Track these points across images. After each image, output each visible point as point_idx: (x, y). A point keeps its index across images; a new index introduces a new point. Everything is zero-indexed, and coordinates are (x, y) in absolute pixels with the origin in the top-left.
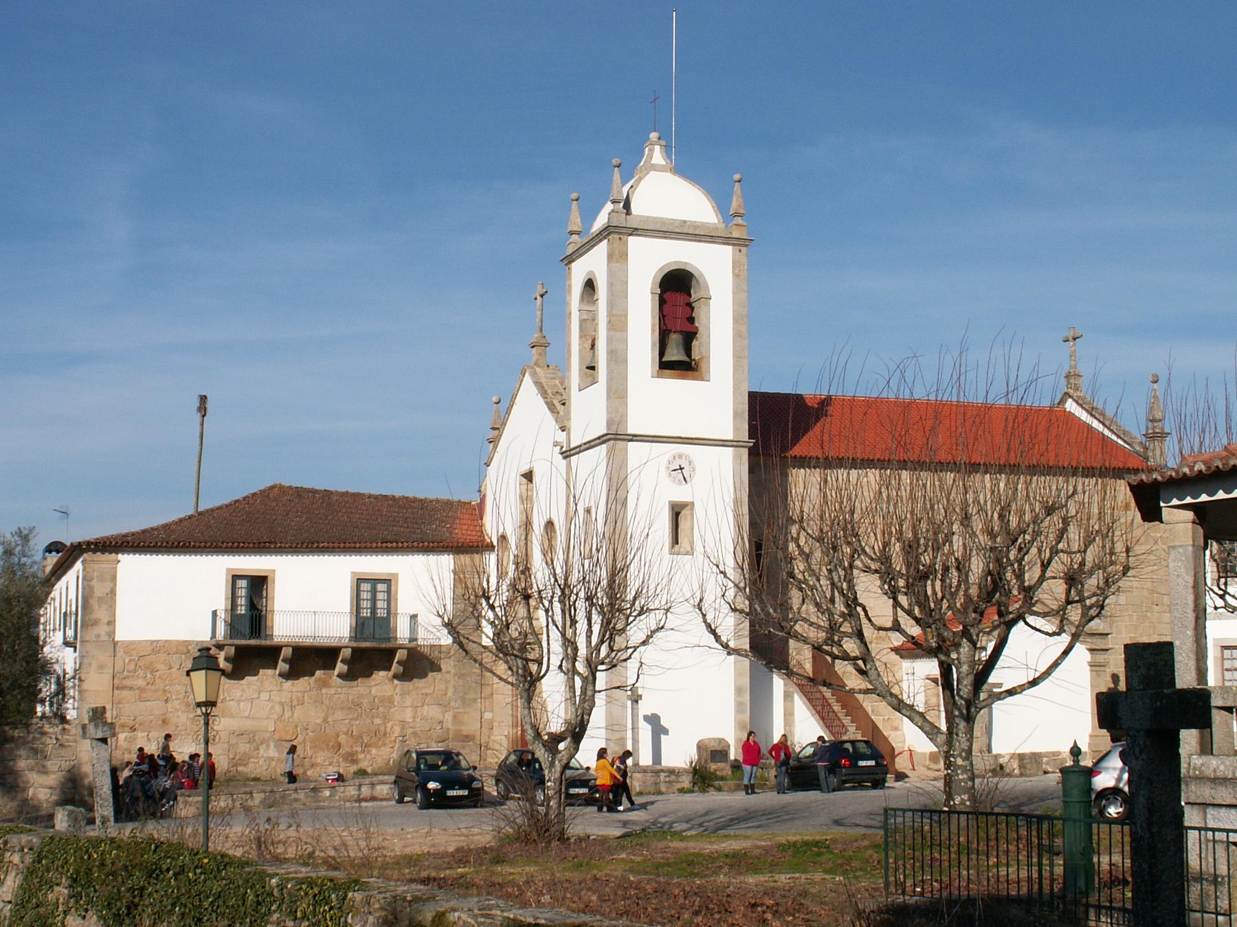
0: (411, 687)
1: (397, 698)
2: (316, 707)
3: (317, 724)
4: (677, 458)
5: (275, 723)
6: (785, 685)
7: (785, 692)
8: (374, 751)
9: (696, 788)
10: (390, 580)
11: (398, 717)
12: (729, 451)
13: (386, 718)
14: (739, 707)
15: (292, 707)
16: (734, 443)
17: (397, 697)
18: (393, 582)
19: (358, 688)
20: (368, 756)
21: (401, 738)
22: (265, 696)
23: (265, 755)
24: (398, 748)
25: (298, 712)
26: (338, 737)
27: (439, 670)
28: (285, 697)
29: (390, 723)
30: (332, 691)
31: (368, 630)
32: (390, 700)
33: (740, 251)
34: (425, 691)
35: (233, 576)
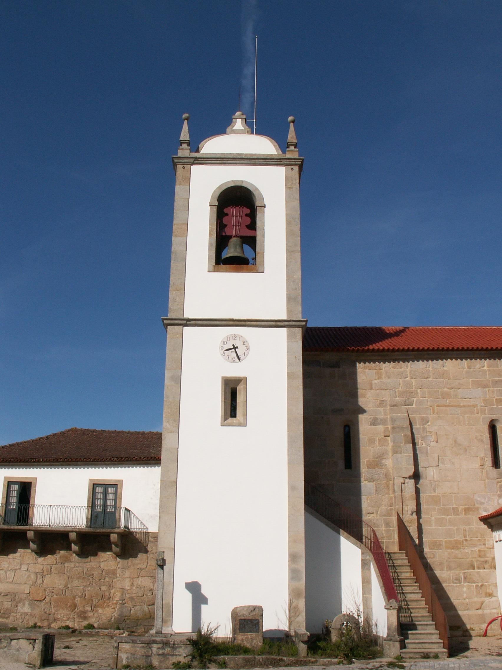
0: (130, 563)
1: (119, 571)
2: (60, 576)
3: (60, 589)
4: (231, 339)
5: (30, 587)
6: (363, 553)
7: (362, 560)
8: (100, 611)
9: (195, 663)
10: (117, 485)
11: (119, 585)
12: (283, 332)
13: (110, 586)
14: (293, 574)
15: (43, 576)
16: (287, 323)
17: (118, 570)
18: (119, 486)
19: (91, 563)
20: (96, 615)
21: (121, 602)
22: (24, 567)
23: (22, 611)
24: (118, 609)
25: (47, 580)
26: (75, 599)
27: (146, 551)
28: (38, 568)
29: (113, 590)
30: (72, 565)
31: (100, 520)
32: (114, 572)
33: (292, 169)
34: (140, 566)
35: (8, 482)
